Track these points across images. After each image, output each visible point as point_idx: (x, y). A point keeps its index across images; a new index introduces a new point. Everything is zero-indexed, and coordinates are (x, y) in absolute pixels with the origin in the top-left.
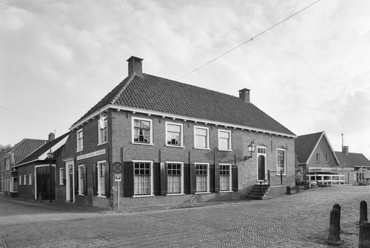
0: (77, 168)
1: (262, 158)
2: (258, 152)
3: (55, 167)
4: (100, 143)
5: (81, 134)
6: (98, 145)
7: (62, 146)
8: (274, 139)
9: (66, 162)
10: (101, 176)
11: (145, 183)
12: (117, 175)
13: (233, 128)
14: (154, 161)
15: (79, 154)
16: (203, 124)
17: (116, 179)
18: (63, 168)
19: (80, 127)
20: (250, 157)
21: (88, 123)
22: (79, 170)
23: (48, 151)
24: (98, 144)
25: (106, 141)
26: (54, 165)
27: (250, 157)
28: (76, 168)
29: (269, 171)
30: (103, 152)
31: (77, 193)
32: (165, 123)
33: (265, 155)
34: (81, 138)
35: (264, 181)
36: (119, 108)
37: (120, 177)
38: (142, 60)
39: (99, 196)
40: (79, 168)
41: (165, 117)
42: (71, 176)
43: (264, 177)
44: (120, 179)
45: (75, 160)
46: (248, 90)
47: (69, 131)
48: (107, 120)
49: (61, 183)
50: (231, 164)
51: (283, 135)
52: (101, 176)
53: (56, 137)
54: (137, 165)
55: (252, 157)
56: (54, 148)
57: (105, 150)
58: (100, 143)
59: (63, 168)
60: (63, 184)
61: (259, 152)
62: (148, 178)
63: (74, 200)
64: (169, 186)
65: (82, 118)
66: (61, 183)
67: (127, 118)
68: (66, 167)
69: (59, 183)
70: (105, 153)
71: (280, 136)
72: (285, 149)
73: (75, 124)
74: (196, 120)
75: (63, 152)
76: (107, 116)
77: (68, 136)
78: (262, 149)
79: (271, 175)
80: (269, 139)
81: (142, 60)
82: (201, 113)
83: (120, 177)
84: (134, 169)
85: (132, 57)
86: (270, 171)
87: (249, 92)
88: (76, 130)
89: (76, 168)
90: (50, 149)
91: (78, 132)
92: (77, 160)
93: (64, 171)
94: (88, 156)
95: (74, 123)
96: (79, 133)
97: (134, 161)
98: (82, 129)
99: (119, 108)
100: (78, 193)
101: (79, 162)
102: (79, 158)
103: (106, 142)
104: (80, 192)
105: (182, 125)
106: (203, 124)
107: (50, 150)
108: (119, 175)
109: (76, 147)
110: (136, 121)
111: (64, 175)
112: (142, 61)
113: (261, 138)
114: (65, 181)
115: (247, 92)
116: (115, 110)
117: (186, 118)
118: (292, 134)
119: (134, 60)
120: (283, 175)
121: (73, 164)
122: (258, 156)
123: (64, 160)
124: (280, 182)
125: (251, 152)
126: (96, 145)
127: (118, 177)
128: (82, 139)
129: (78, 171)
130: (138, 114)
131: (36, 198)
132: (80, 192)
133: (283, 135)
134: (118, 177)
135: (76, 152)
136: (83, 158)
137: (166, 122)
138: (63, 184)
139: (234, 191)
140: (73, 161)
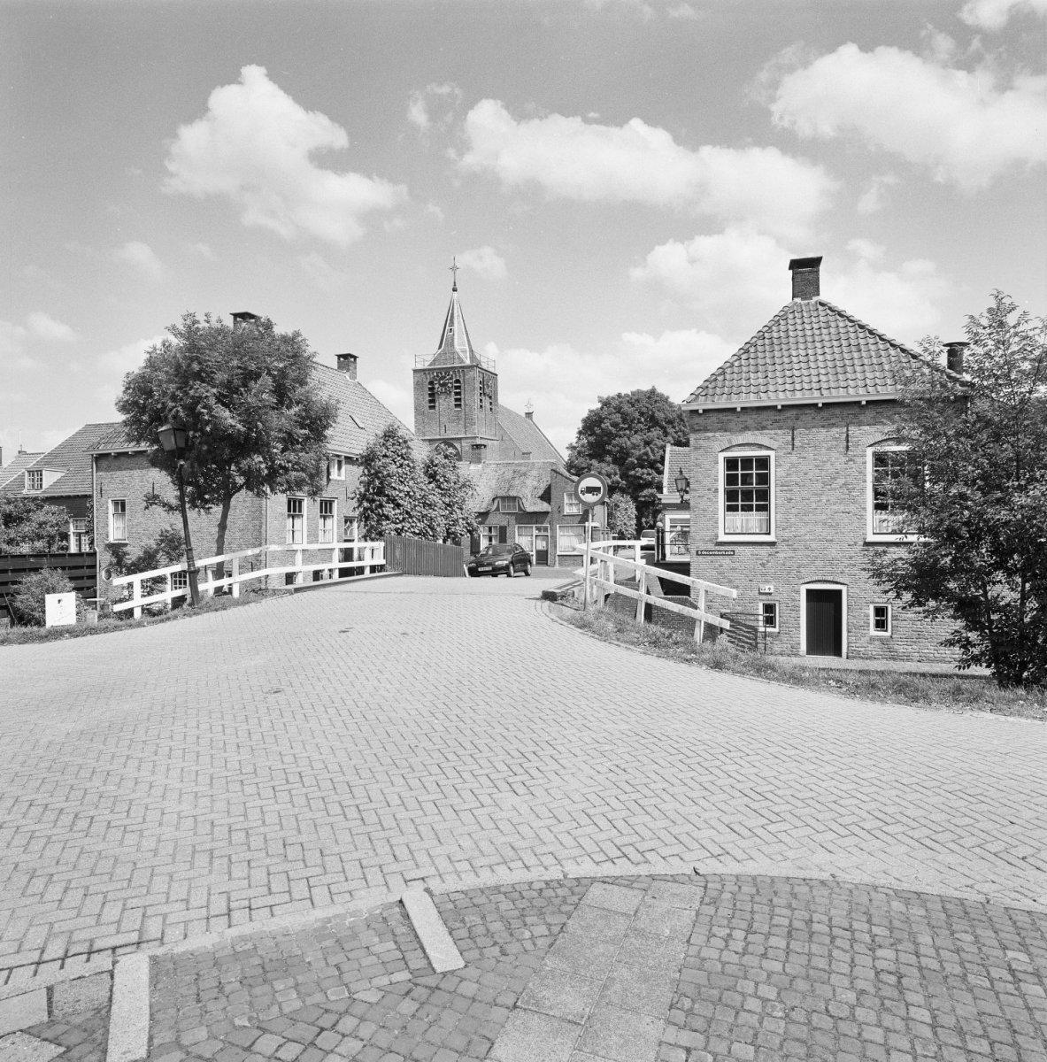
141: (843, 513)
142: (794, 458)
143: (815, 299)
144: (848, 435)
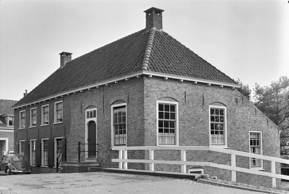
10: (44, 151)
11: (164, 137)
33: (95, 119)
36: (151, 74)
38: (163, 11)
39: (43, 166)
41: (168, 78)
51: (222, 84)
52: (33, 151)
81: (163, 11)
82: (175, 68)
85: (152, 9)
99: (151, 74)
112: (162, 12)
116: (147, 76)
118: (232, 81)
119: (154, 13)
122: (86, 123)
124: (77, 159)
133: (222, 84)
141: (202, 134)
142: (185, 107)
143: (161, 30)
144: (203, 99)
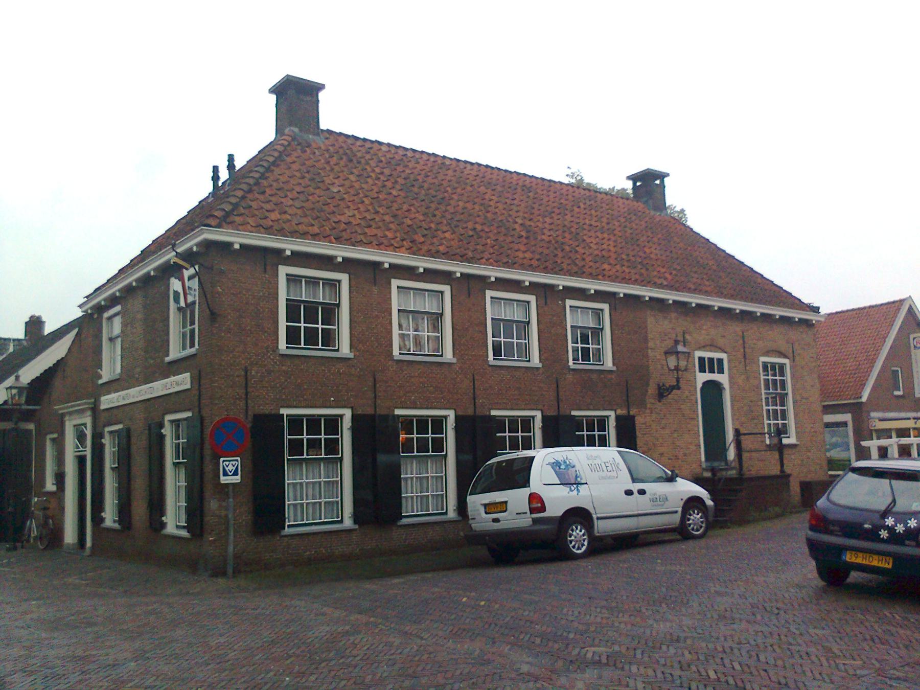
0: (101, 436)
1: (712, 390)
2: (700, 371)
3: (31, 431)
4: (175, 353)
5: (117, 323)
6: (167, 359)
7: (58, 361)
8: (753, 331)
9: (67, 418)
12: (227, 463)
13: (614, 294)
14: (352, 408)
15: (113, 385)
16: (515, 286)
17: (225, 474)
18: (55, 436)
19: (113, 301)
20: (673, 388)
21: (197, 253)
22: (107, 441)
23: (10, 381)
24: (168, 355)
25: (192, 345)
26: (31, 426)
27: (673, 388)
28: (97, 436)
29: (737, 433)
30: (182, 381)
31: (98, 520)
32: (390, 283)
33: (723, 379)
34: (117, 337)
35: (723, 464)
37: (237, 468)
40: (167, 424)
42: (81, 460)
43: (725, 450)
44: (235, 473)
45: (95, 410)
46: (662, 176)
47: (79, 313)
48: (197, 279)
49: (50, 486)
50: (612, 414)
53: (48, 329)
54: (296, 423)
55: (679, 388)
56: (30, 373)
57: (187, 375)
58: (175, 353)
59: (55, 436)
60: (54, 488)
61: (702, 370)
62: (335, 465)
63: (89, 543)
64: (288, 501)
65: (146, 254)
66: (50, 486)
67: (265, 271)
68: (67, 432)
69: (43, 486)
70: (188, 386)
71: (766, 317)
72: (785, 357)
73: (121, 271)
74: (493, 273)
75: (57, 383)
76: (197, 267)
77: (76, 330)
78: (711, 360)
79: (747, 442)
80: (736, 328)
83: (237, 468)
84: (287, 437)
86: (742, 431)
87: (662, 182)
88: (100, 309)
89: (97, 436)
90: (15, 374)
91: (106, 315)
92: (102, 407)
93: (59, 444)
94: (136, 394)
95: (97, 286)
96: (110, 318)
97: (284, 411)
98: (118, 308)
100: (102, 520)
101: (106, 414)
102: (108, 401)
103: (193, 351)
104: (110, 517)
105: (446, 289)
106: (515, 286)
107: (17, 378)
108: (234, 463)
109: (100, 367)
110: (291, 279)
111: (60, 460)
113: (707, 329)
114: (60, 478)
115: (658, 182)
117: (458, 268)
120: (785, 441)
121: (88, 420)
122: (699, 385)
123: (61, 409)
125: (677, 369)
126: (163, 361)
127: (230, 467)
128: (119, 339)
129: (102, 446)
130: (299, 258)
131: (830, 473)
132: (110, 517)
134: (230, 467)
135: (100, 382)
136: (120, 404)
137: (393, 281)
138: (54, 488)
139: (193, 535)
140: (89, 413)
